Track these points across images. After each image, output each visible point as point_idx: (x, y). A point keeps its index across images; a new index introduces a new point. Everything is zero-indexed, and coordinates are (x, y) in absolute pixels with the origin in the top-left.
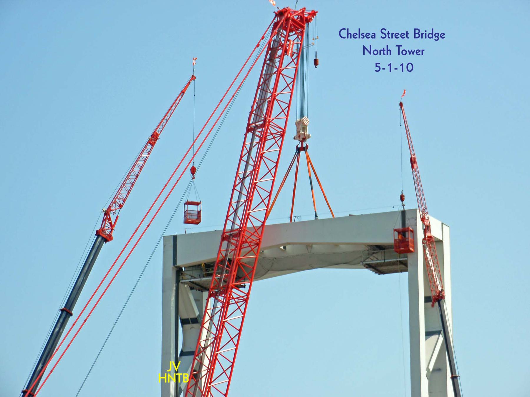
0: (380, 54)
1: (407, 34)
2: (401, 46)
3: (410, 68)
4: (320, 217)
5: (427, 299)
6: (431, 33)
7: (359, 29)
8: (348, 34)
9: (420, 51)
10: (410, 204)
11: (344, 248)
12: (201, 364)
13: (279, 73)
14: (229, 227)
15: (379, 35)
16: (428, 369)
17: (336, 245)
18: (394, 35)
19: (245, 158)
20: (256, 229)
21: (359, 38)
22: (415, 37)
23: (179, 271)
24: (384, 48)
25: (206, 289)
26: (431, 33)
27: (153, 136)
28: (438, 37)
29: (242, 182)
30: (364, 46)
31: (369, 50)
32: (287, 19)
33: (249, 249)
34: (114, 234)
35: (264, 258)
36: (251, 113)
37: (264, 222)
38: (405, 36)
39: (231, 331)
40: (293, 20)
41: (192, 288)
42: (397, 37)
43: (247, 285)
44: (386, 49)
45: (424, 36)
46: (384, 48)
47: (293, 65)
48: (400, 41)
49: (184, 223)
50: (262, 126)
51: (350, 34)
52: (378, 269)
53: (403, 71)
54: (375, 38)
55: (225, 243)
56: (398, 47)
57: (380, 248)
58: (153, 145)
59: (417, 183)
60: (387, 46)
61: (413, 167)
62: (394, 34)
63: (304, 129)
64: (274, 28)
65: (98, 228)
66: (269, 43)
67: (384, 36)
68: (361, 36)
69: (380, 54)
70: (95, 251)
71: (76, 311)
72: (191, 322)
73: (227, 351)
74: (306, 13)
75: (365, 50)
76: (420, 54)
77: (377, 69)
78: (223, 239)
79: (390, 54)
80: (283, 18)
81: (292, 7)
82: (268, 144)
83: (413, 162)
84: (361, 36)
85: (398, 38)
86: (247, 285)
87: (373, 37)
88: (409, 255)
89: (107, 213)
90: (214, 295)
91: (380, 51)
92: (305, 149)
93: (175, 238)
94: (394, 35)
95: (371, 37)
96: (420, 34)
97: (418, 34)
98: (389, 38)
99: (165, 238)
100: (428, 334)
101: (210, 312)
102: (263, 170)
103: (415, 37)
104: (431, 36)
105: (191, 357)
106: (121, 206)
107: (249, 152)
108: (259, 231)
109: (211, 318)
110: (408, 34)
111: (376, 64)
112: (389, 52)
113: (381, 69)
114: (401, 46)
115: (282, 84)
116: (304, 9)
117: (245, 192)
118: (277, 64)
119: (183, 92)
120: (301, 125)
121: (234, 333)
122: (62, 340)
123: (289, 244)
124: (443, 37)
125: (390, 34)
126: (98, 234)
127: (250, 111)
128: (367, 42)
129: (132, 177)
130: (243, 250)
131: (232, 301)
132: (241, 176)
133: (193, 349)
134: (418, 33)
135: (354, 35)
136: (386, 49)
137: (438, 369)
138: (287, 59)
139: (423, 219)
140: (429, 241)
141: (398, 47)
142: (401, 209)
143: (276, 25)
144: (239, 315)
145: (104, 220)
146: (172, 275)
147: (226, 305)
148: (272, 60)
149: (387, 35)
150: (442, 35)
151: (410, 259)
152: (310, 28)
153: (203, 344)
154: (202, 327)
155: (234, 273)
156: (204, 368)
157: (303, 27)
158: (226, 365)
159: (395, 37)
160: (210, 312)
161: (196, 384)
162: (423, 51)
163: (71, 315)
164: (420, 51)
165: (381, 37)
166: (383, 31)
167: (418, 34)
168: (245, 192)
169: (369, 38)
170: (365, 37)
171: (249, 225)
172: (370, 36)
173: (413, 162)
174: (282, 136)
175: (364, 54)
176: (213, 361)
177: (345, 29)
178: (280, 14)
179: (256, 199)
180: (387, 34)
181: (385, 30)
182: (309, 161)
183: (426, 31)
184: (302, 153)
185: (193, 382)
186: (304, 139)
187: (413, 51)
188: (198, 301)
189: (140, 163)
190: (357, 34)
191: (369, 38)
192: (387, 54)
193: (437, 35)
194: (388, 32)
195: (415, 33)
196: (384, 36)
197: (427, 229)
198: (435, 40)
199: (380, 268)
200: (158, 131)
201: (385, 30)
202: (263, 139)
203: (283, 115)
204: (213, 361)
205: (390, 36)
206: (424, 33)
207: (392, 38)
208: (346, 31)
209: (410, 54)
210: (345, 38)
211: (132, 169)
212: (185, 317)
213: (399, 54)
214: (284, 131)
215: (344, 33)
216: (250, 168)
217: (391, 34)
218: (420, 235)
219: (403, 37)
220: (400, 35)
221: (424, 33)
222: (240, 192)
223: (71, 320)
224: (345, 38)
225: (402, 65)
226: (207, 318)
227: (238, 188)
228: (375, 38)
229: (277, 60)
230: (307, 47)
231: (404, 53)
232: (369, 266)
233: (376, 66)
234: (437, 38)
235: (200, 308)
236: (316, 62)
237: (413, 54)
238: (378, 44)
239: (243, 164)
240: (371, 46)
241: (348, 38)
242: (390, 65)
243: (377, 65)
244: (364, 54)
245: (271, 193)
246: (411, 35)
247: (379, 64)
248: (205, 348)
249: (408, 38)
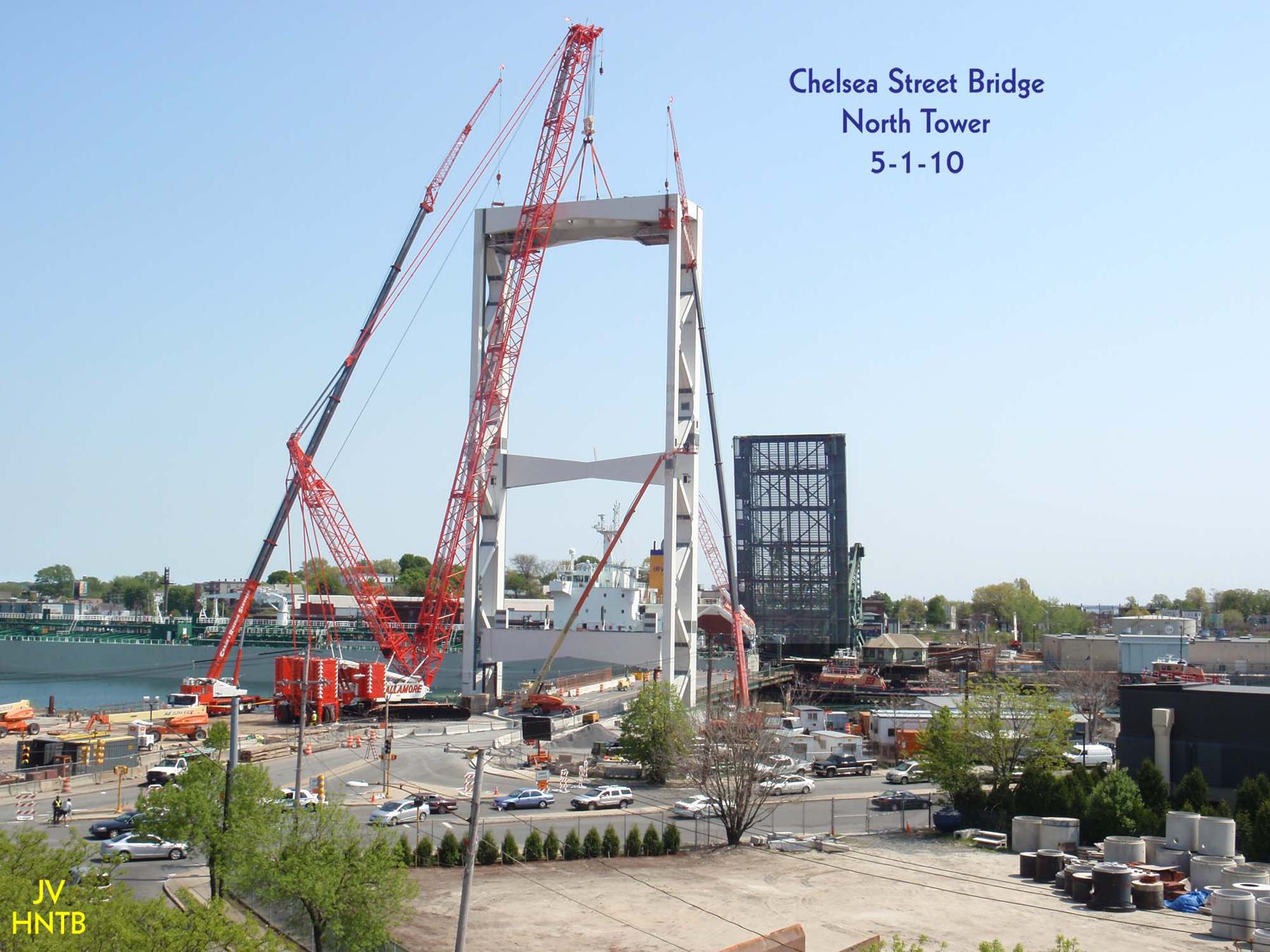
0: (884, 131)
1: (953, 81)
2: (934, 110)
3: (955, 163)
4: (600, 198)
5: (683, 267)
6: (1011, 78)
7: (839, 70)
8: (811, 82)
9: (978, 122)
10: (673, 190)
11: (619, 223)
12: (503, 313)
13: (571, 78)
14: (528, 204)
15: (885, 83)
16: (681, 322)
17: (613, 221)
18: (921, 86)
19: (542, 148)
20: (550, 206)
21: (838, 91)
22: (972, 90)
23: (487, 238)
24: (892, 116)
25: (509, 253)
26: (1011, 78)
27: (466, 127)
28: (1026, 89)
29: (539, 168)
30: (845, 111)
31: (857, 121)
32: (579, 34)
33: (544, 222)
34: (434, 207)
35: (555, 230)
36: (548, 111)
37: (556, 201)
38: (948, 86)
39: (527, 287)
40: (584, 35)
41: (497, 252)
42: (929, 89)
43: (541, 251)
44: (897, 117)
45: (993, 86)
46: (892, 116)
47: (583, 72)
48: (933, 99)
50: (557, 122)
51: (817, 82)
52: (646, 241)
53: (938, 171)
54: (875, 91)
55: (525, 216)
56: (925, 114)
57: (647, 224)
58: (466, 134)
59: (679, 173)
60: (901, 110)
61: (676, 159)
63: (590, 125)
64: (568, 42)
65: (422, 201)
66: (564, 54)
67: (896, 86)
68: (842, 87)
69: (884, 131)
70: (419, 220)
71: (403, 268)
73: (524, 302)
75: (857, 121)
76: (978, 130)
77: (877, 165)
78: (523, 213)
79: (908, 131)
80: (576, 33)
81: (583, 24)
82: (561, 136)
83: (676, 155)
84: (842, 87)
85: (932, 90)
86: (541, 251)
87: (872, 88)
88: (670, 231)
89: (429, 189)
90: (515, 258)
91: (884, 122)
92: (590, 142)
93: (484, 211)
94: (921, 86)
95: (865, 89)
96: (985, 81)
97: (977, 81)
98: (909, 91)
99: (476, 211)
100: (683, 294)
101: (511, 271)
102: (556, 158)
103: (972, 90)
104: (1009, 86)
105: (496, 307)
106: (440, 184)
107: (546, 143)
108: (552, 207)
109: (512, 277)
110: (956, 81)
111: (875, 154)
112: (905, 125)
113: (887, 166)
114: (934, 110)
115: (573, 88)
116: (593, 26)
117: (541, 175)
118: (570, 71)
119: (492, 92)
120: (588, 122)
121: (530, 288)
123: (576, 218)
124: (1039, 88)
125: (911, 81)
126: (422, 206)
128: (853, 102)
129: (450, 161)
130: (538, 223)
131: (529, 263)
132: (539, 162)
133: (497, 301)
134: (979, 80)
135: (827, 84)
136: (897, 117)
137: (689, 322)
138: (578, 67)
139: (682, 203)
140: (688, 221)
141: (925, 114)
142: (665, 193)
143: (570, 38)
144: (534, 274)
145: (427, 195)
146: (481, 241)
147: (524, 266)
148: (566, 67)
149: (905, 84)
150: (1037, 85)
151: (671, 234)
152: (598, 42)
153: (505, 297)
154: (505, 283)
155: (531, 241)
156: (506, 316)
157: (592, 41)
158: (523, 314)
159: (925, 88)
160: (511, 271)
161: (499, 328)
162: (986, 122)
163: (400, 270)
164: (978, 122)
165: (891, 89)
166: (896, 74)
167: (977, 81)
168: (541, 175)
169: (863, 90)
170: (852, 88)
171: (544, 202)
172: (864, 87)
173: (676, 155)
174: (572, 130)
175: (845, 130)
176: (513, 311)
177: (804, 70)
178: (574, 29)
179: (550, 182)
180: (906, 81)
181: (901, 71)
182: (593, 151)
183: (997, 75)
184: (588, 145)
185: (497, 326)
186: (590, 134)
187: (962, 123)
188: (502, 262)
189: (460, 143)
190: (832, 82)
191: (863, 90)
192: (901, 131)
193: (1024, 85)
194: (908, 76)
195: (972, 80)
196: (896, 86)
197: (685, 210)
198: (1021, 96)
199: (648, 241)
200: (471, 124)
201: (901, 71)
202: (557, 133)
203: (573, 113)
204: (513, 311)
205: (912, 86)
206: (993, 81)
207: (917, 91)
208: (807, 74)
209: (955, 129)
210: (804, 91)
211: (450, 154)
212: (491, 275)
213: (929, 130)
214: (574, 126)
215: (802, 80)
216: (546, 156)
217: (914, 82)
218: (680, 215)
219: (943, 88)
220: (935, 85)
221: (993, 81)
222: (538, 175)
223: (400, 275)
224: (804, 91)
225: (937, 156)
226: (509, 276)
227: (536, 172)
228: (875, 91)
229: (570, 67)
230: (595, 57)
231: (944, 126)
232: (638, 239)
233: (875, 159)
234: (1024, 93)
235: (503, 268)
236: (601, 70)
237: (963, 129)
238: (880, 105)
239: (540, 152)
240: (861, 111)
241: (811, 91)
242: (907, 156)
243: (877, 156)
244: (845, 130)
245: (562, 177)
246: (963, 83)
247: (881, 153)
248: (507, 300)
249: (954, 91)
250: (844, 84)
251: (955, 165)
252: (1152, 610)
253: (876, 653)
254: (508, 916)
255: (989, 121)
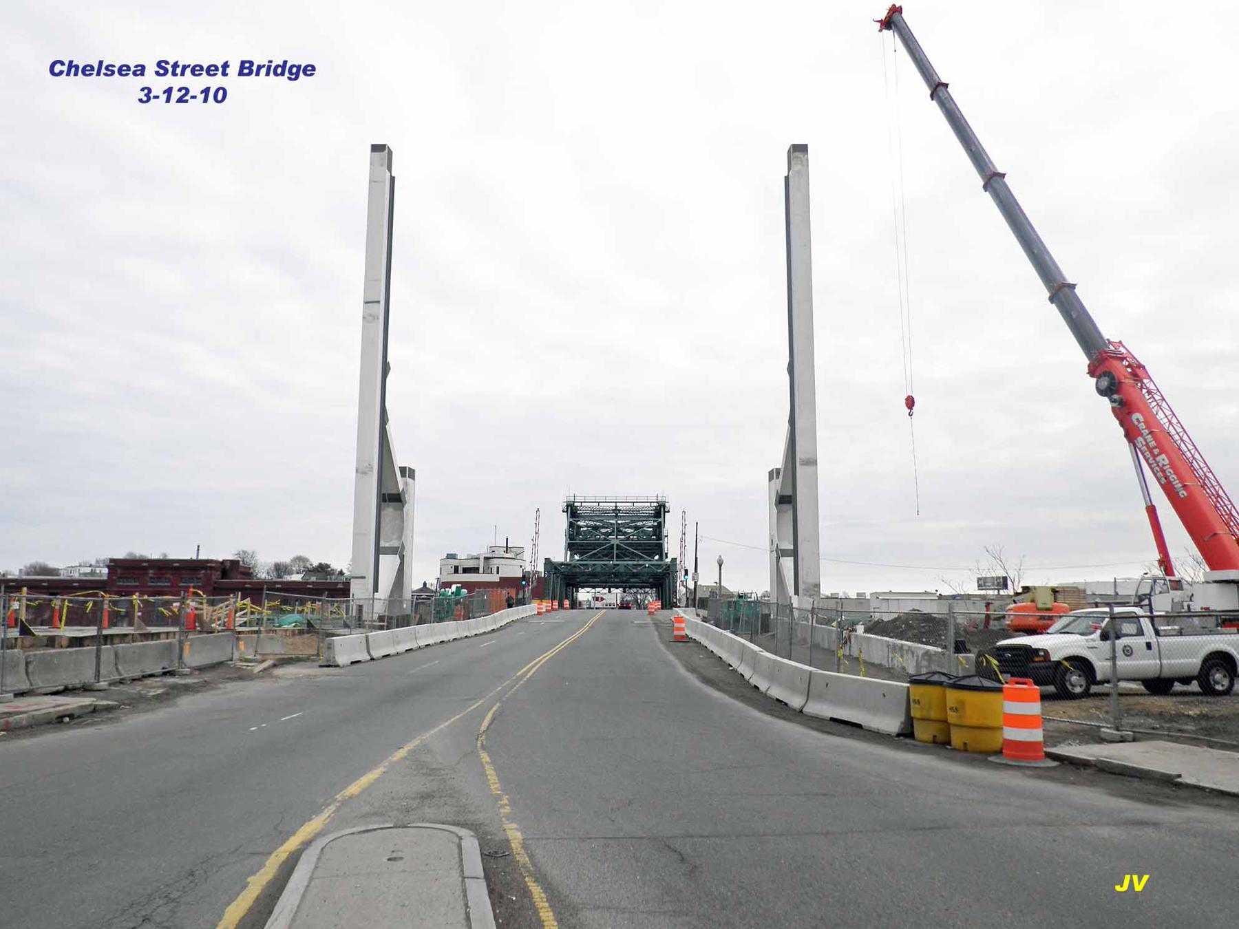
45: (263, 71)
49: (806, 145)
62: (189, 66)
72: (407, 469)
74: (957, 669)
122: (449, 829)
125: (178, 66)
127: (323, 562)
150: (309, 70)
193: (294, 70)
205: (179, 71)
217: (181, 67)
250: (107, 68)
251: (220, 97)
255: (895, 11)
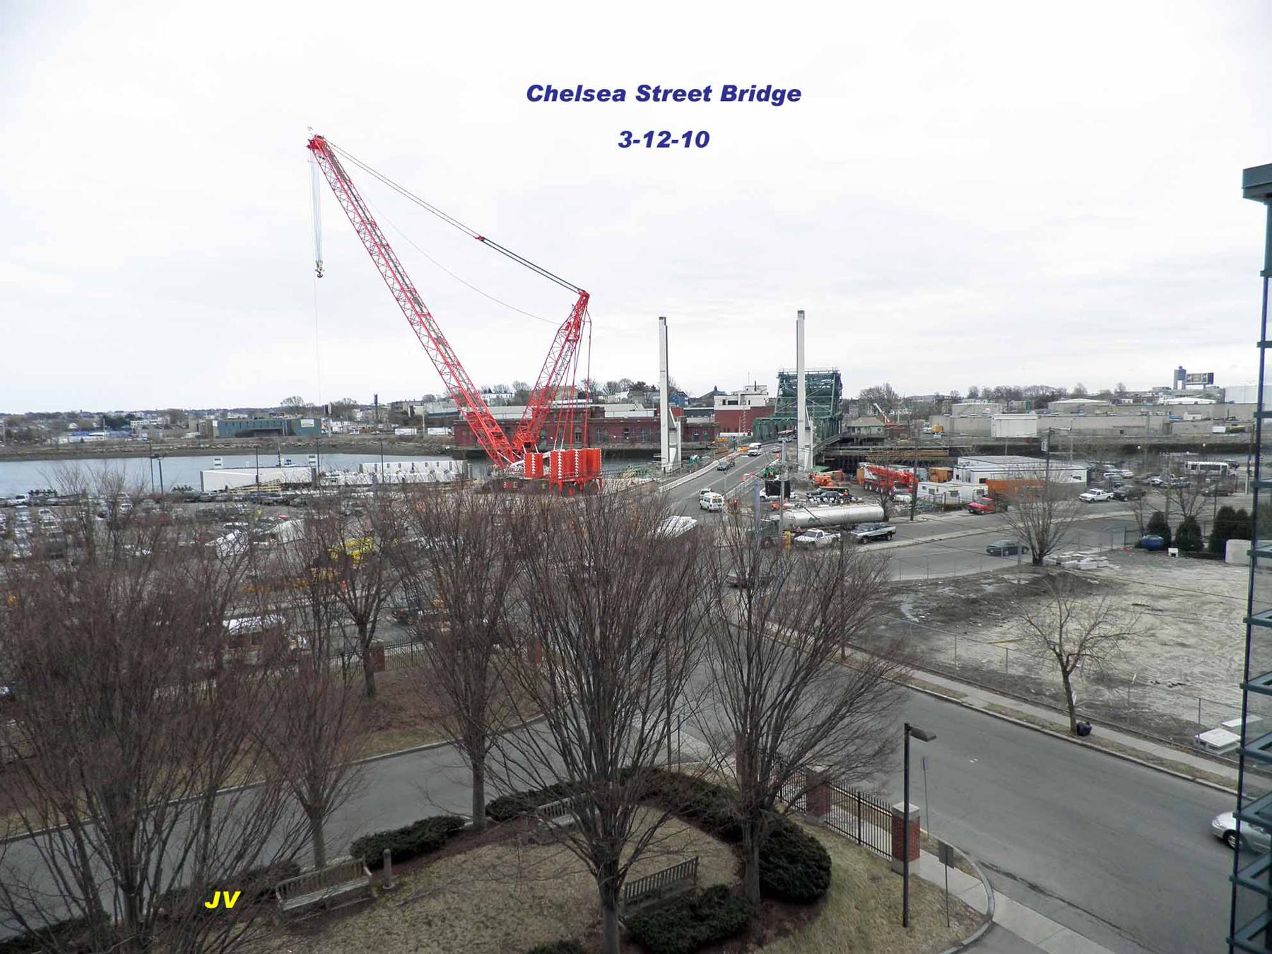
54: (622, 99)
84: (582, 96)
125: (660, 91)
150: (795, 95)
193: (778, 95)
217: (662, 92)
246: (716, 94)
250: (586, 93)
251: (702, 141)
252: (1073, 397)
253: (856, 430)
254: (1126, 683)
